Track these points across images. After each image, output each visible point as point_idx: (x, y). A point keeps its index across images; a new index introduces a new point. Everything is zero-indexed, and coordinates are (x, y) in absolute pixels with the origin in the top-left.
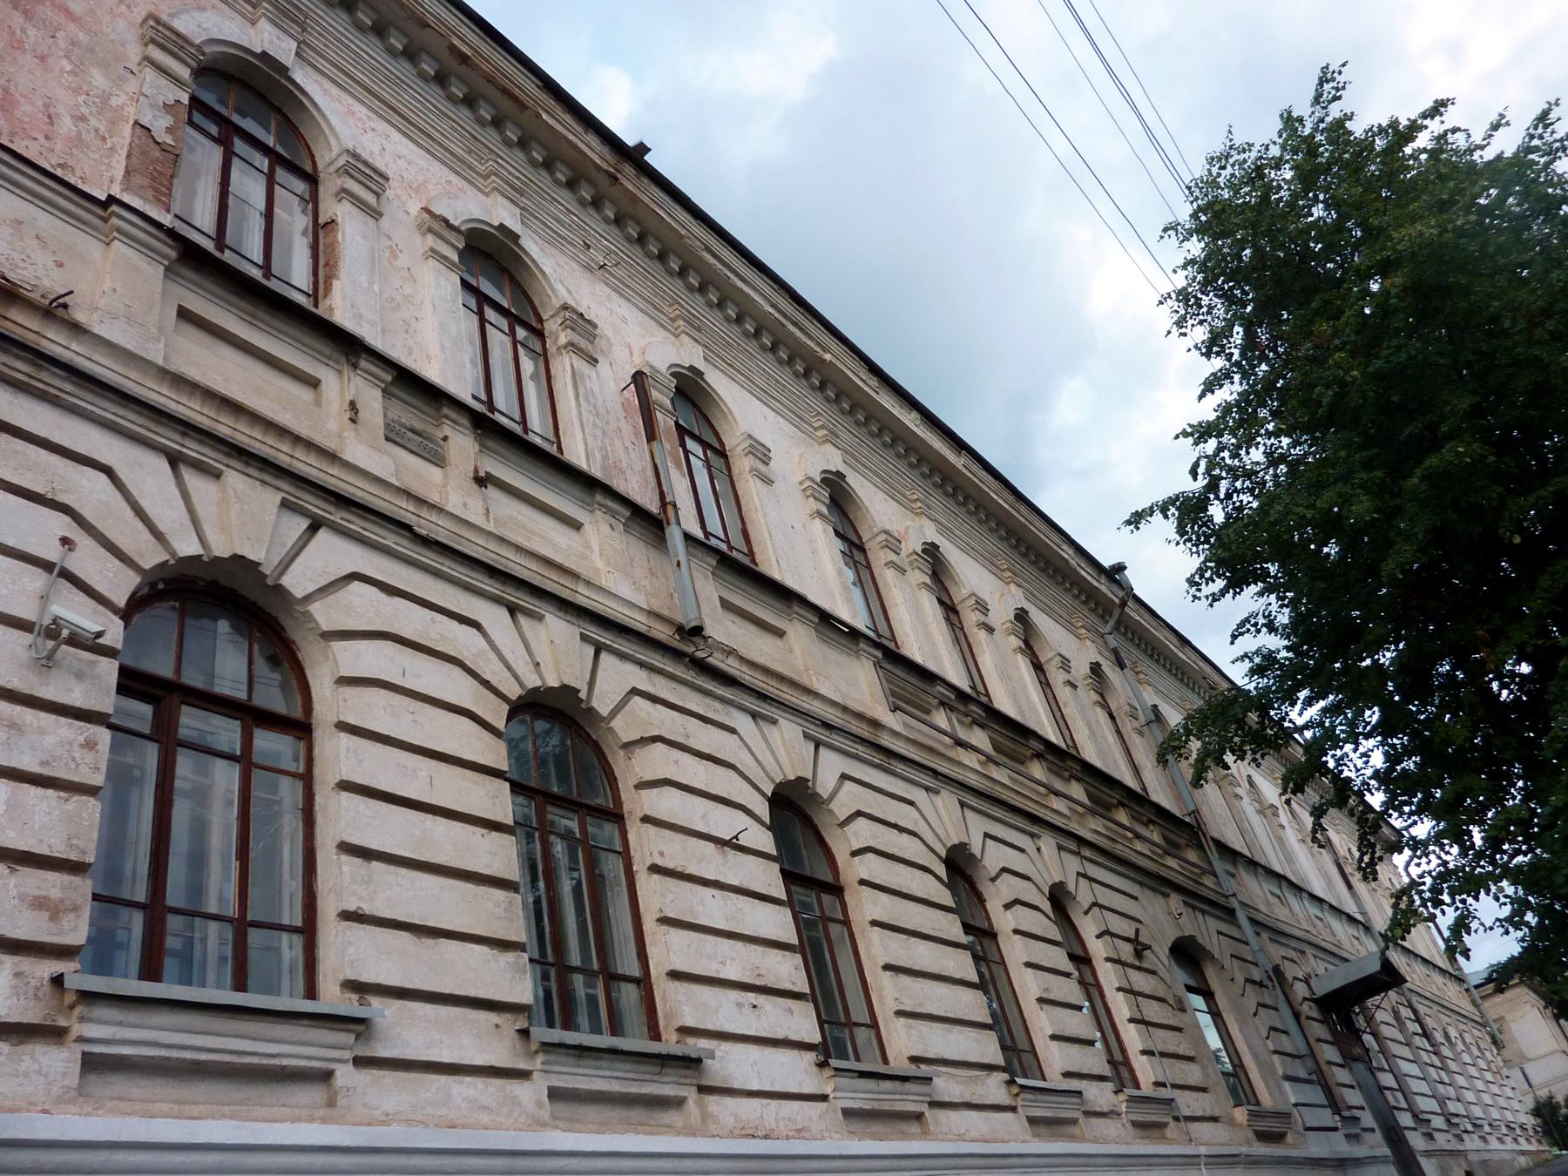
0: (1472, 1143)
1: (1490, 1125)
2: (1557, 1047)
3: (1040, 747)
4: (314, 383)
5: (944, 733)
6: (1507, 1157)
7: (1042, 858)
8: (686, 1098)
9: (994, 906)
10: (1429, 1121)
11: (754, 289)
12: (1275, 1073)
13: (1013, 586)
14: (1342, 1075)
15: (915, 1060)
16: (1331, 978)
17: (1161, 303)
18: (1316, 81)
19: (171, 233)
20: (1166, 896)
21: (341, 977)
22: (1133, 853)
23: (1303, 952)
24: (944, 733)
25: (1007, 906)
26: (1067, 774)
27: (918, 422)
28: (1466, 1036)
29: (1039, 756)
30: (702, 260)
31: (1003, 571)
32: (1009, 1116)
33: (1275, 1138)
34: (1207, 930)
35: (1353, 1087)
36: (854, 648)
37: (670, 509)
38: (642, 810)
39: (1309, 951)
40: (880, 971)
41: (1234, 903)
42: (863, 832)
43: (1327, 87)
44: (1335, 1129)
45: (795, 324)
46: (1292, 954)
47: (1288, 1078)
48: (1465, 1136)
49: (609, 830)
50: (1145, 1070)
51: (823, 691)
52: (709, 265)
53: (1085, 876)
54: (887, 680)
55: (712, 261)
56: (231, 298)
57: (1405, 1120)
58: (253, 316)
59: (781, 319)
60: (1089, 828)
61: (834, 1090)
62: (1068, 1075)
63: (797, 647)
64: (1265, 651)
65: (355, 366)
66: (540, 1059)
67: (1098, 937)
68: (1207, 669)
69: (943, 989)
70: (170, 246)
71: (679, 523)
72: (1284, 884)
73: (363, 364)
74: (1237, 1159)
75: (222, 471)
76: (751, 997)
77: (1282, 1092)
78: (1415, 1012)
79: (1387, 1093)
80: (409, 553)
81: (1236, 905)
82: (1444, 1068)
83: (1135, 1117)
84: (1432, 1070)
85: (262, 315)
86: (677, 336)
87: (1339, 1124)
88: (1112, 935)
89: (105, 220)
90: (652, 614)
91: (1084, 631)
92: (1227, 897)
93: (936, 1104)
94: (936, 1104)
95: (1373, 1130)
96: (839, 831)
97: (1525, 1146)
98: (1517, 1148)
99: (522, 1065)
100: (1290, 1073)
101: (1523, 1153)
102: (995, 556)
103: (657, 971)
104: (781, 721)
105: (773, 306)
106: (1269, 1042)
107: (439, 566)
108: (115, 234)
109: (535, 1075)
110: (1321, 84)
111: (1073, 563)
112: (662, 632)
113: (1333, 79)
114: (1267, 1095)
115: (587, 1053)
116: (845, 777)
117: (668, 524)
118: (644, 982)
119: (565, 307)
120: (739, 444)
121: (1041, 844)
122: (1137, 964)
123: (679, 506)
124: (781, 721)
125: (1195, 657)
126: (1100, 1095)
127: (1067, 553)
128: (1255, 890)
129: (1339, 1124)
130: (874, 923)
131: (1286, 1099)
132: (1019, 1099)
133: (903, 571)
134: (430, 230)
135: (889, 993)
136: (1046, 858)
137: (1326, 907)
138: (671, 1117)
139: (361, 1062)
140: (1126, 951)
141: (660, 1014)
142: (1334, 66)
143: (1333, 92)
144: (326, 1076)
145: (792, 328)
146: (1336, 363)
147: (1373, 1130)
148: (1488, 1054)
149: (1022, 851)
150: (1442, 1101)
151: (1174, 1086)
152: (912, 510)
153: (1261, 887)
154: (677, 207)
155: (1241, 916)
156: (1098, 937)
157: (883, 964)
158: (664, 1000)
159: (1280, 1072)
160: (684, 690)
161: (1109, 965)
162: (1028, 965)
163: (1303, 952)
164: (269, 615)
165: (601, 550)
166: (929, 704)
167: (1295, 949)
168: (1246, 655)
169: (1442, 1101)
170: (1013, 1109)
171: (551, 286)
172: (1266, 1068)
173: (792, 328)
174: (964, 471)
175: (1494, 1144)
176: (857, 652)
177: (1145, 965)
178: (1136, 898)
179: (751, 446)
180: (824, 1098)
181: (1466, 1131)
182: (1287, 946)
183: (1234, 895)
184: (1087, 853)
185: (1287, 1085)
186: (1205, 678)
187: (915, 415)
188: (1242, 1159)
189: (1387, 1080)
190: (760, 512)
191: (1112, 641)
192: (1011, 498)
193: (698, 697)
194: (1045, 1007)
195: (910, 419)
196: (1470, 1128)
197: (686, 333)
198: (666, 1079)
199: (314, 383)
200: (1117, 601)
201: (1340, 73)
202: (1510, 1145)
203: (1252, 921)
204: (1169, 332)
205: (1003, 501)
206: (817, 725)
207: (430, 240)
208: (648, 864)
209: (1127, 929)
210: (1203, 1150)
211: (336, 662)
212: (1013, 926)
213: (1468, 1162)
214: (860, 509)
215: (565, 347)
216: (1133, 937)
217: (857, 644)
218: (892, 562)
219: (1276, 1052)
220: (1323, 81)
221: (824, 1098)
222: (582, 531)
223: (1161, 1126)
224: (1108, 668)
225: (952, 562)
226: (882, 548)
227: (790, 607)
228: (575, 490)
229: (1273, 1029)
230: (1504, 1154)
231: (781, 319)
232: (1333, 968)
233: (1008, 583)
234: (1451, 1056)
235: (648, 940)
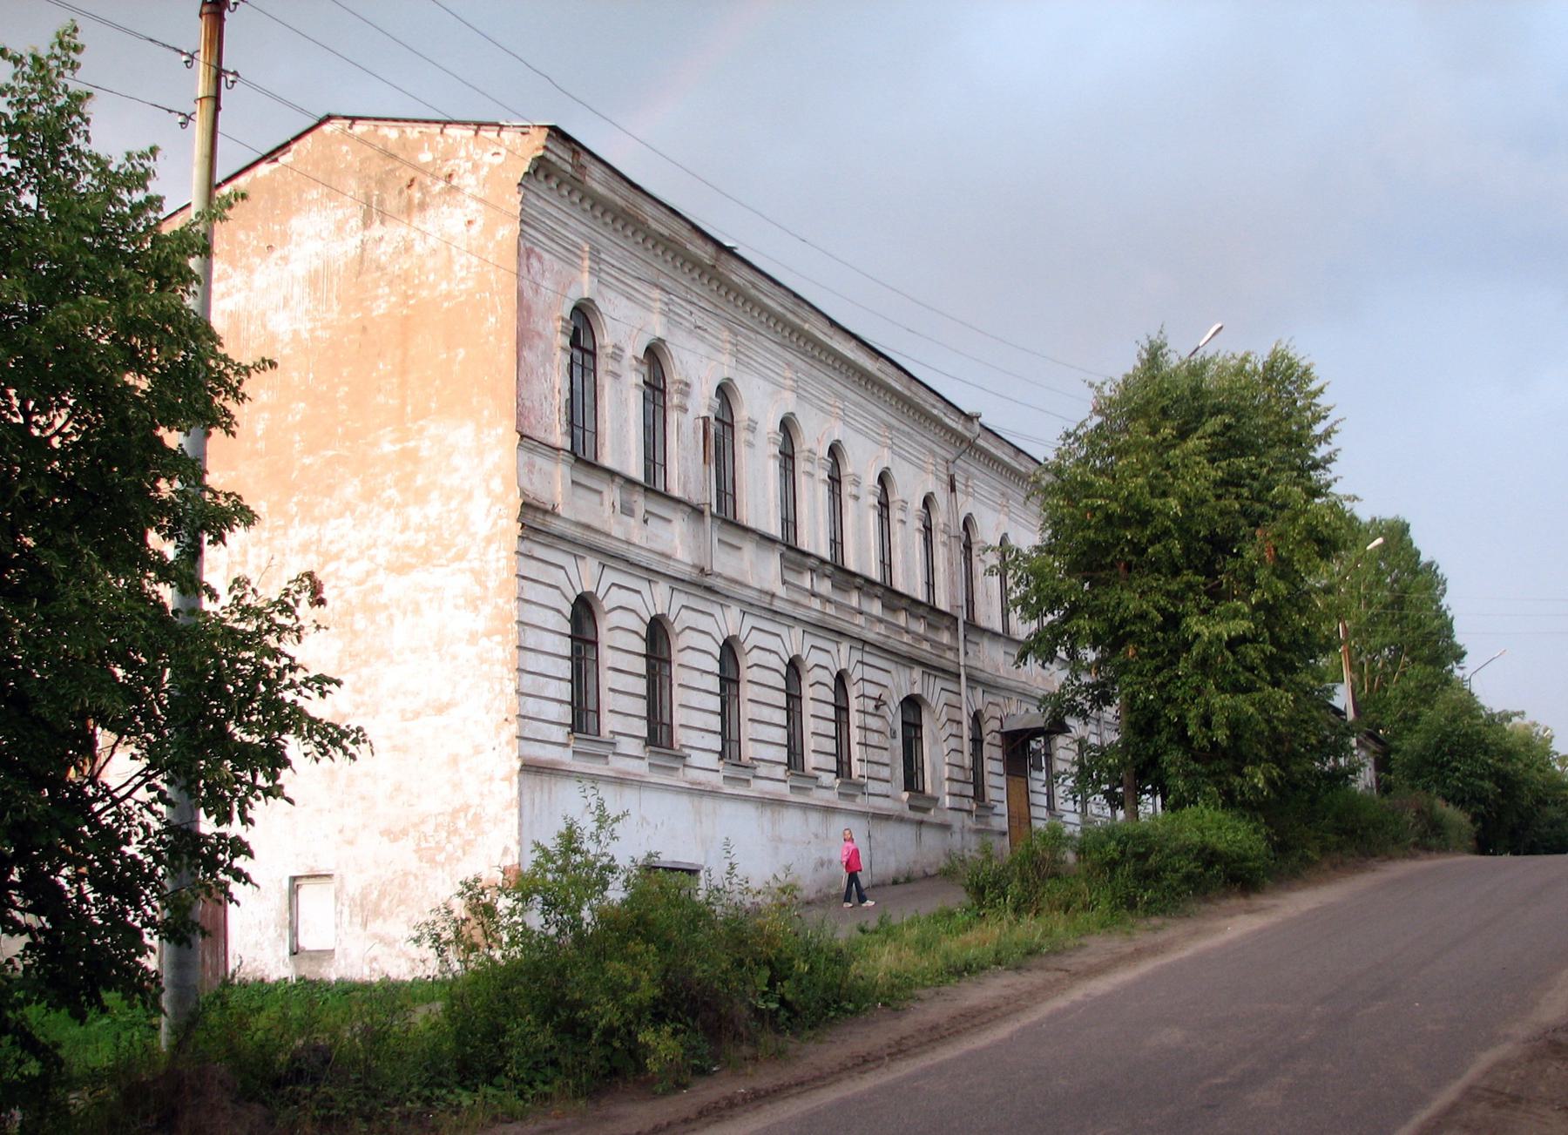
4: (600, 493)
9: (805, 684)
15: (752, 759)
20: (911, 668)
32: (782, 784)
33: (851, 797)
42: (756, 657)
49: (733, 686)
50: (857, 769)
53: (862, 663)
62: (815, 769)
69: (627, 699)
76: (703, 733)
93: (755, 777)
116: (753, 628)
118: (670, 726)
126: (828, 779)
135: (607, 700)
139: (614, 754)
140: (871, 705)
144: (606, 757)
149: (828, 652)
160: (698, 600)
170: (785, 781)
199: (600, 493)
207: (1526, 721)
223: (854, 796)
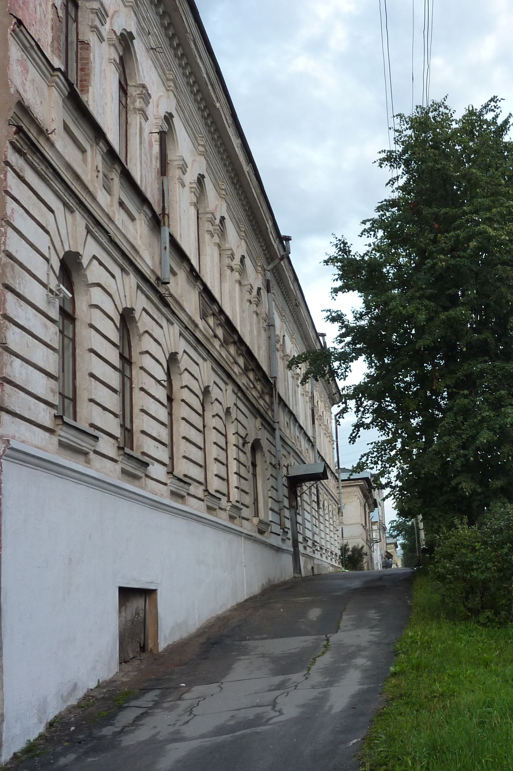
0: (317, 555)
1: (326, 550)
2: (360, 521)
3: (236, 338)
5: (210, 327)
6: (327, 565)
7: (226, 394)
8: (142, 477)
10: (308, 541)
11: (203, 64)
12: (267, 506)
13: (243, 242)
14: (287, 513)
16: (297, 470)
17: (380, 153)
18: (490, 99)
19: (70, 85)
20: (256, 418)
21: (90, 422)
22: (250, 395)
23: (289, 453)
24: (210, 327)
25: (213, 416)
26: (240, 352)
27: (239, 145)
28: (330, 507)
29: (234, 343)
30: (189, 45)
31: (242, 231)
34: (264, 436)
35: (288, 519)
36: (194, 283)
37: (166, 217)
38: (141, 364)
39: (292, 453)
40: (181, 438)
41: (276, 426)
43: (493, 104)
44: (279, 535)
45: (212, 85)
46: (286, 453)
47: (271, 510)
48: (316, 551)
51: (187, 310)
52: (191, 48)
54: (202, 304)
55: (193, 47)
56: (71, 108)
57: (300, 538)
58: (76, 119)
59: (208, 82)
60: (242, 381)
61: (170, 483)
62: (217, 491)
63: (180, 283)
64: (339, 313)
65: (97, 144)
66: (121, 457)
67: (234, 434)
68: (299, 295)
70: (67, 90)
71: (169, 226)
72: (292, 417)
73: (101, 144)
74: (251, 538)
75: (75, 211)
77: (268, 516)
78: (318, 491)
79: (298, 525)
80: (106, 246)
81: (277, 428)
82: (318, 519)
83: (230, 513)
84: (314, 519)
85: (79, 120)
86: (167, 90)
87: (281, 534)
88: (239, 435)
89: (52, 76)
90: (153, 272)
91: (260, 269)
92: (274, 422)
94: (188, 494)
95: (289, 539)
96: (179, 376)
97: (334, 563)
98: (331, 563)
99: (117, 459)
100: (273, 508)
101: (332, 566)
102: (240, 222)
103: (136, 429)
104: (175, 325)
105: (207, 74)
106: (269, 492)
107: (111, 251)
108: (54, 84)
109: (119, 462)
110: (490, 101)
111: (269, 230)
112: (153, 280)
113: (496, 102)
114: (263, 514)
115: (131, 458)
117: (164, 225)
119: (144, 86)
120: (176, 160)
121: (227, 388)
122: (242, 449)
123: (170, 217)
124: (175, 325)
125: (297, 288)
127: (269, 225)
128: (282, 418)
129: (281, 534)
130: (183, 419)
131: (268, 519)
132: (206, 497)
133: (213, 236)
134: (114, 45)
136: (228, 395)
137: (302, 432)
138: (137, 482)
141: (134, 445)
142: (499, 98)
143: (493, 108)
145: (210, 87)
146: (440, 258)
147: (289, 539)
148: (335, 517)
150: (314, 534)
151: (242, 504)
152: (219, 194)
153: (284, 418)
154: (191, 15)
155: (277, 432)
156: (234, 434)
157: (183, 436)
158: (138, 441)
159: (270, 507)
161: (235, 447)
162: (215, 443)
163: (289, 453)
164: (69, 270)
165: (141, 235)
166: (208, 312)
167: (287, 451)
168: (330, 311)
169: (314, 534)
171: (138, 68)
172: (266, 503)
173: (210, 87)
174: (247, 174)
175: (324, 559)
176: (194, 285)
177: (244, 450)
178: (247, 417)
179: (183, 165)
180: (166, 484)
181: (317, 550)
182: (285, 449)
183: (278, 422)
184: (239, 395)
185: (270, 512)
186: (296, 300)
187: (239, 141)
188: (253, 538)
189: (299, 519)
190: (178, 204)
191: (269, 275)
192: (259, 191)
193: (156, 311)
194: (217, 462)
195: (236, 142)
196: (319, 549)
197: (173, 92)
198: (141, 470)
199: (83, 151)
200: (279, 256)
201: (500, 101)
202: (329, 561)
203: (281, 438)
204: (375, 162)
205: (255, 192)
206: (183, 327)
208: (140, 386)
209: (243, 433)
210: (245, 531)
211: (91, 297)
212: (214, 426)
213: (314, 564)
214: (204, 196)
215: (139, 110)
216: (244, 436)
217: (196, 282)
218: (210, 231)
219: (270, 497)
220: (492, 100)
221: (166, 484)
222: (134, 222)
224: (263, 292)
225: (208, 197)
226: (208, 221)
227: (182, 262)
228: (137, 201)
229: (272, 487)
230: (326, 564)
231: (208, 82)
232: (298, 464)
233: (241, 239)
234: (322, 515)
235: (134, 416)
